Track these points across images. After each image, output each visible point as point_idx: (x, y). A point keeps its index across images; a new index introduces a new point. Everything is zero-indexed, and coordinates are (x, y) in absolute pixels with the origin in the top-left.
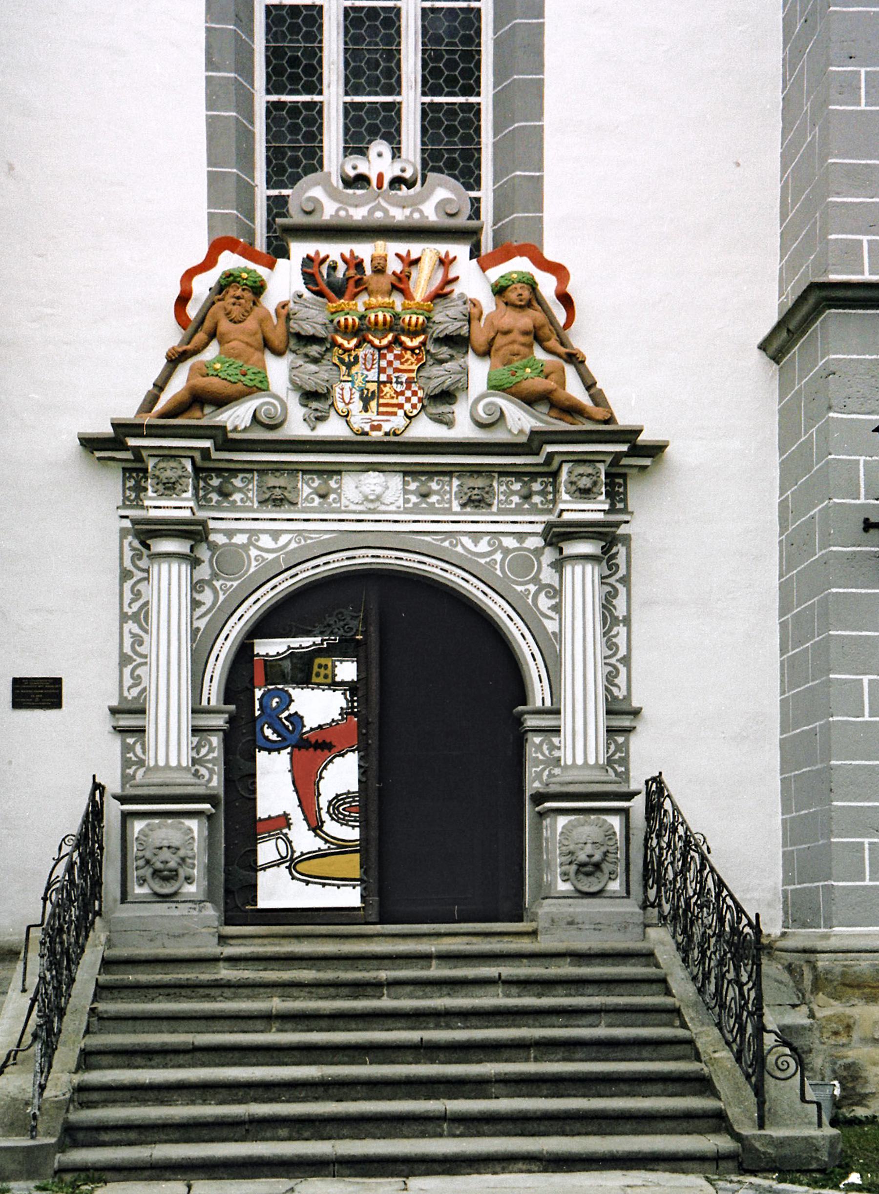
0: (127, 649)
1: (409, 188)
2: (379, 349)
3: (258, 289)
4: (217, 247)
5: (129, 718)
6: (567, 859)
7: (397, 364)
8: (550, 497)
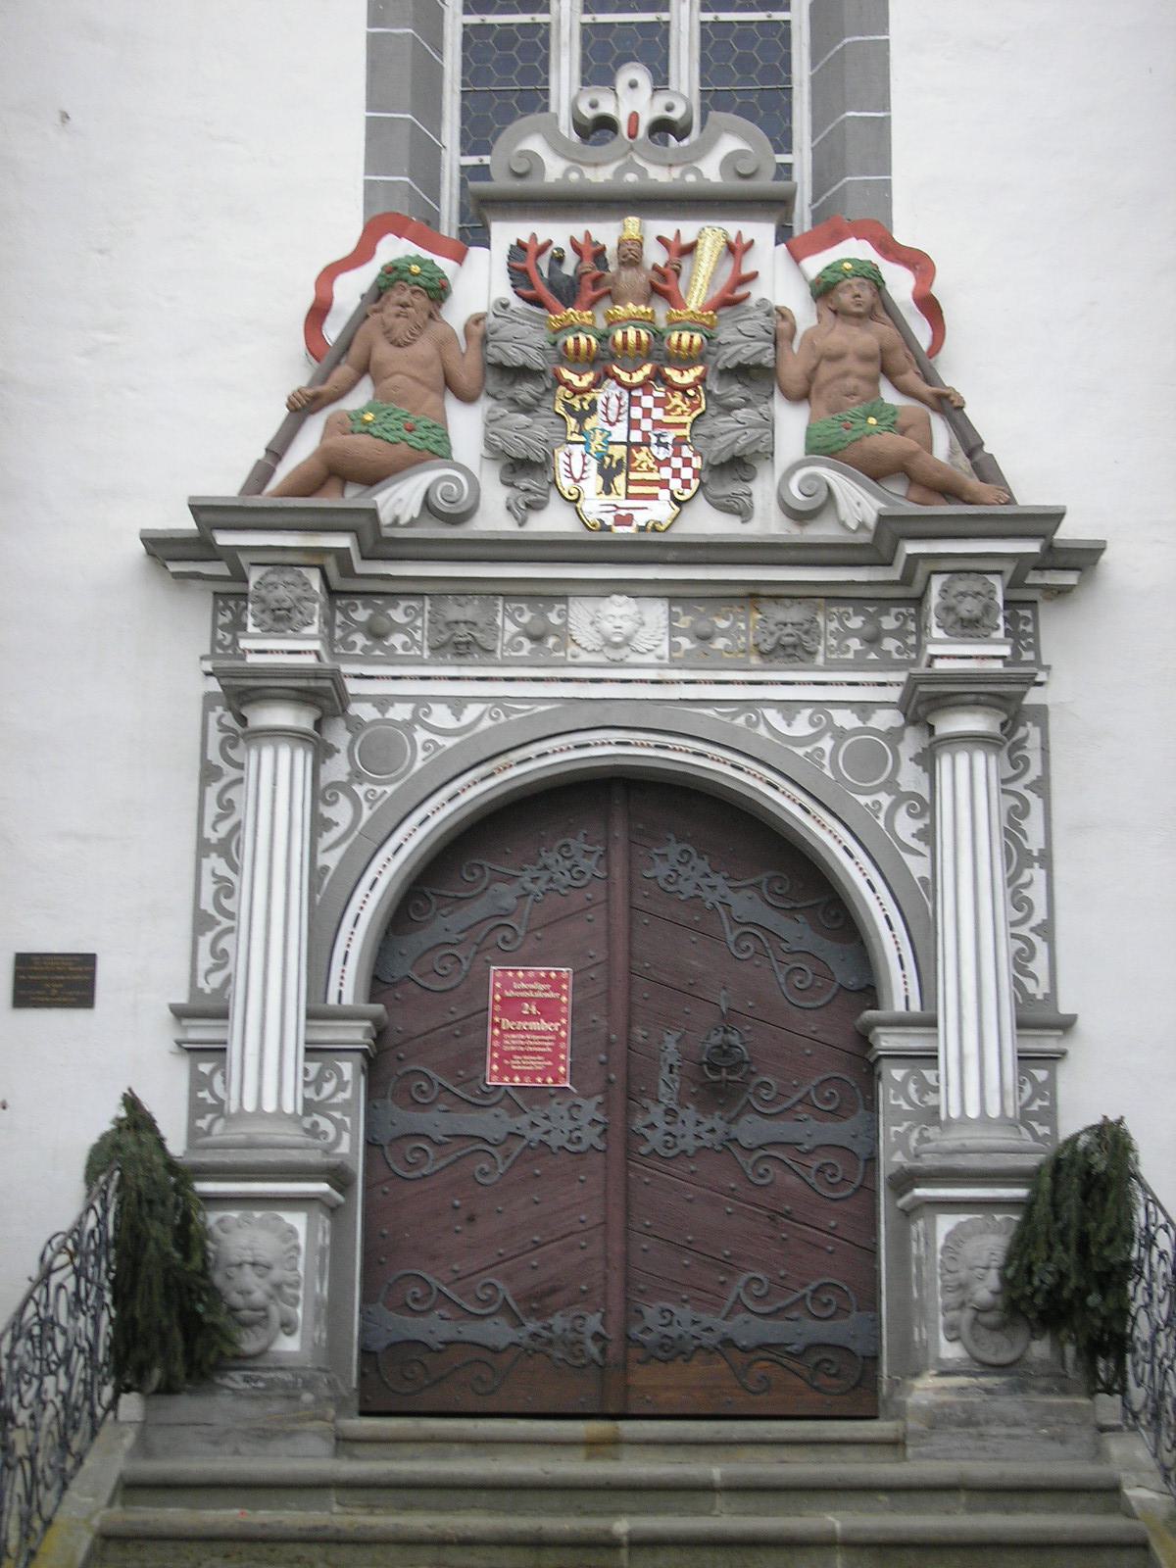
0: (207, 904)
1: (679, 140)
2: (630, 388)
3: (438, 292)
4: (373, 231)
5: (203, 1022)
6: (953, 1298)
7: (658, 414)
8: (912, 640)
